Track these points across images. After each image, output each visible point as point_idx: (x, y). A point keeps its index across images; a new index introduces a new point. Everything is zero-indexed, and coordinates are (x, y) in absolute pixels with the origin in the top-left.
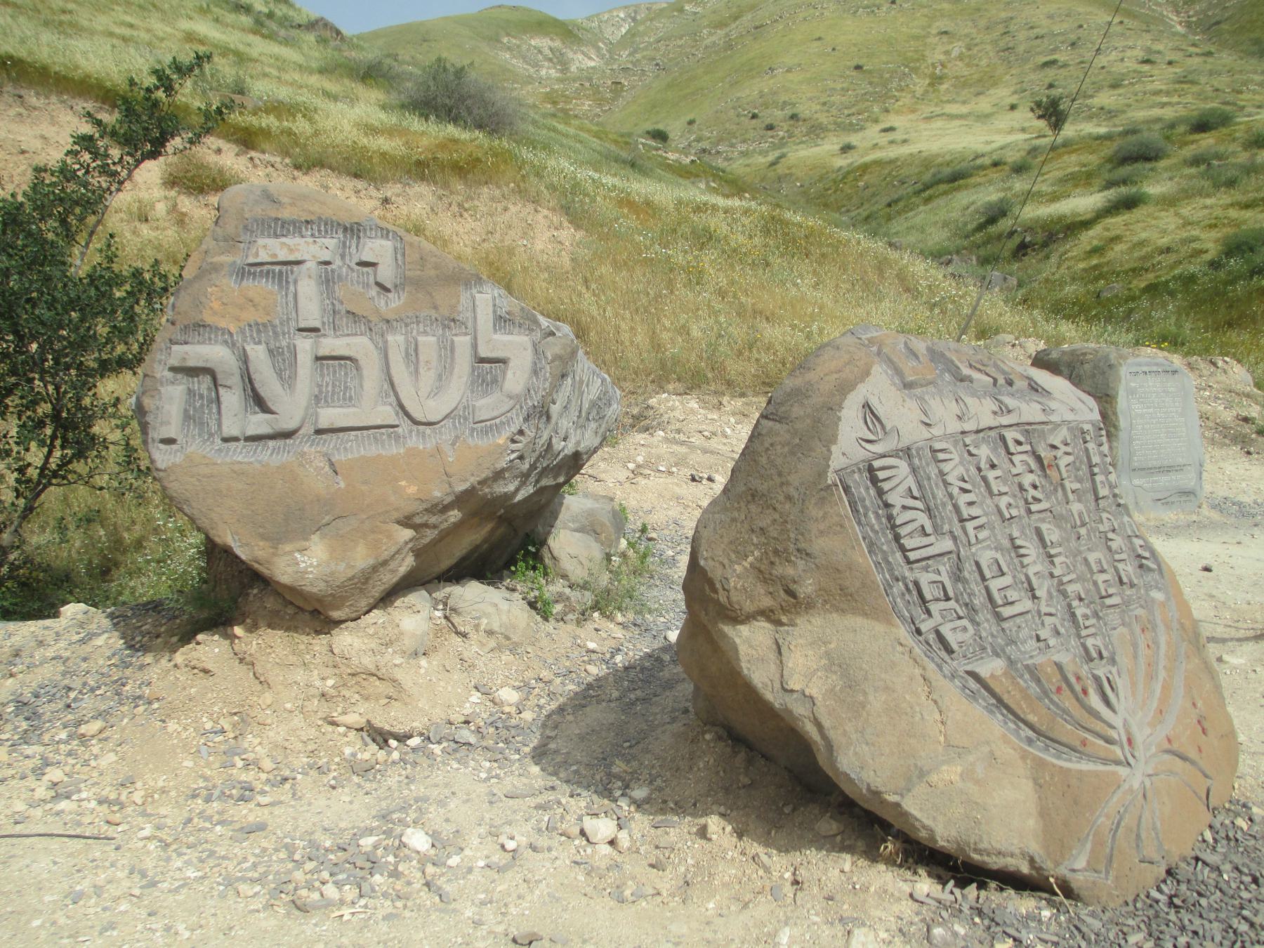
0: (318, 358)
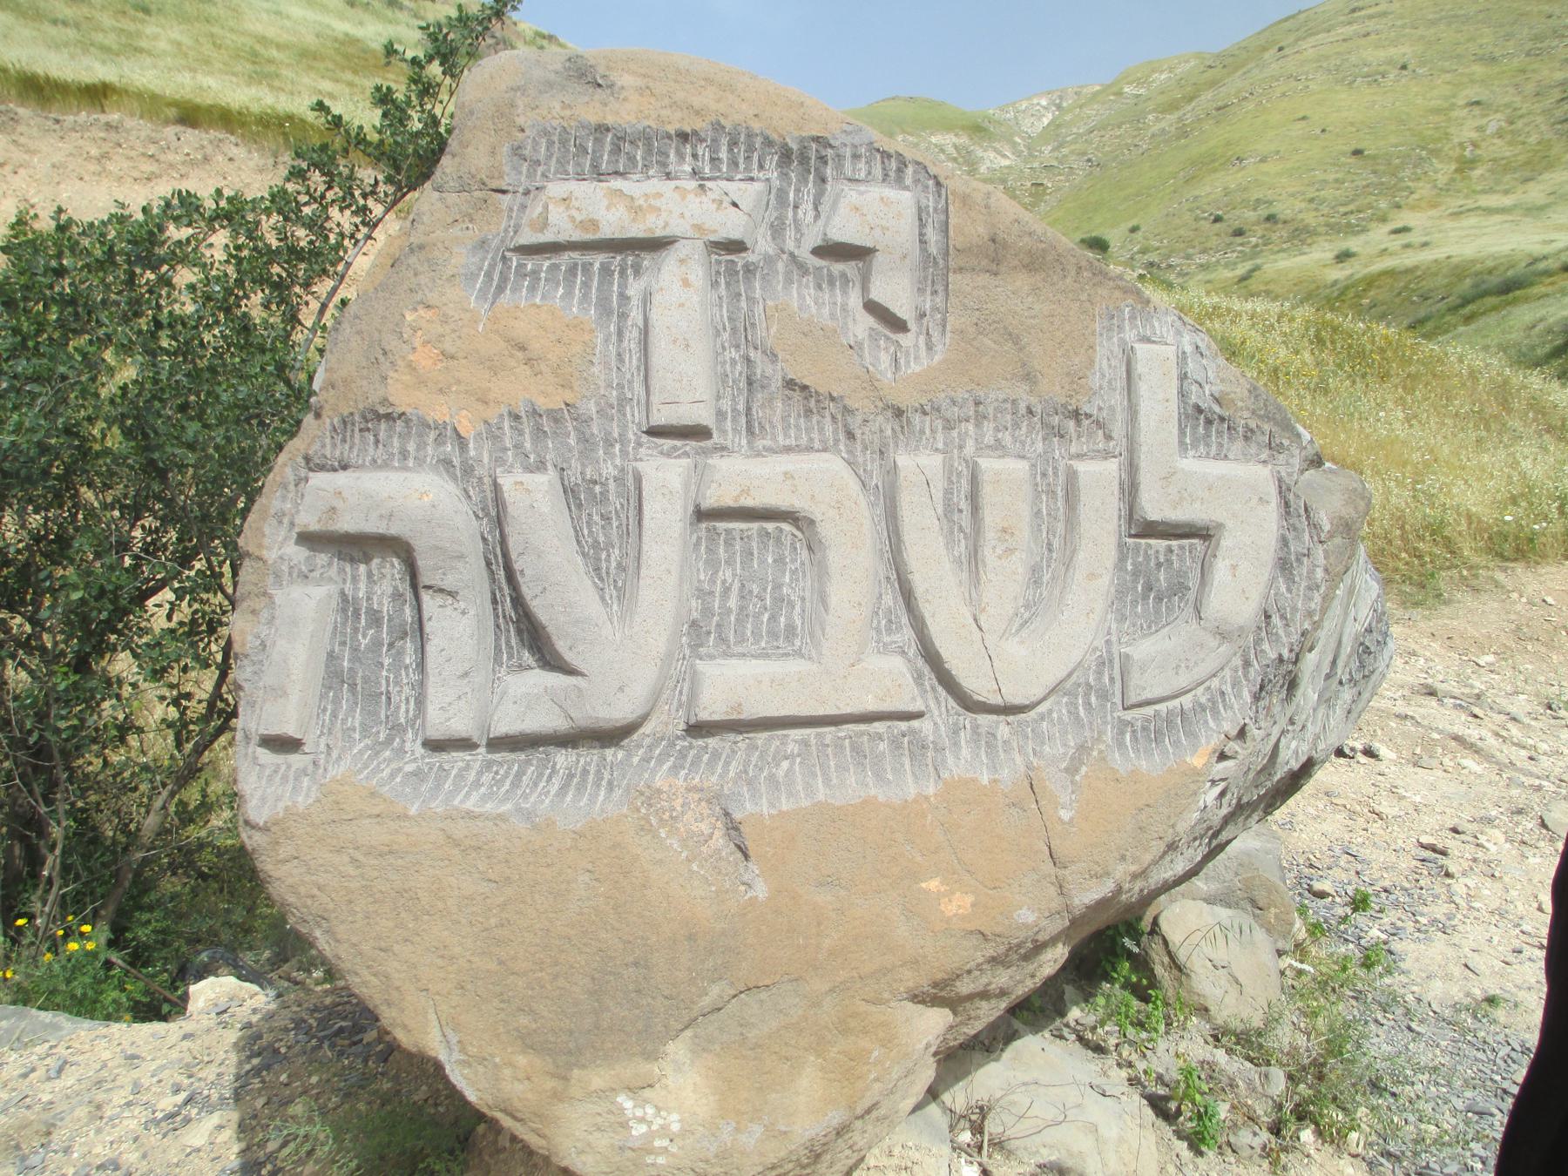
0: (702, 515)
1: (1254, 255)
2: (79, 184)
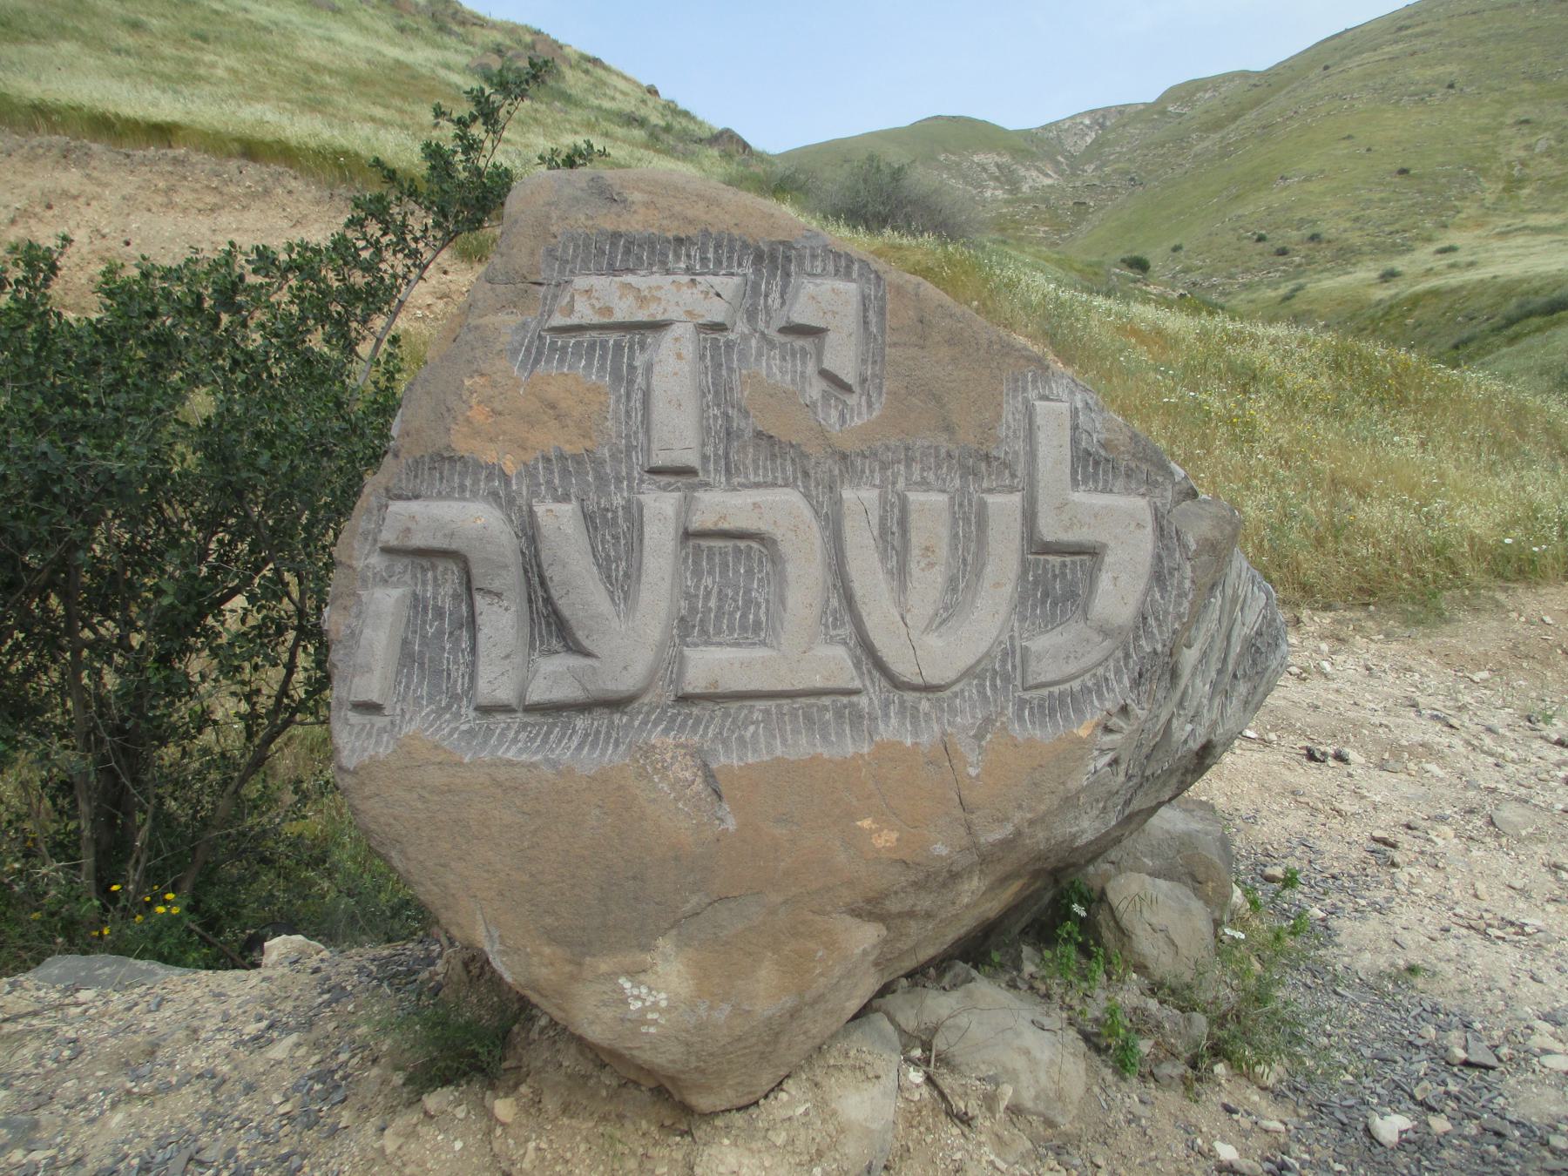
0: (687, 535)
1: (1298, 275)
2: (147, 215)
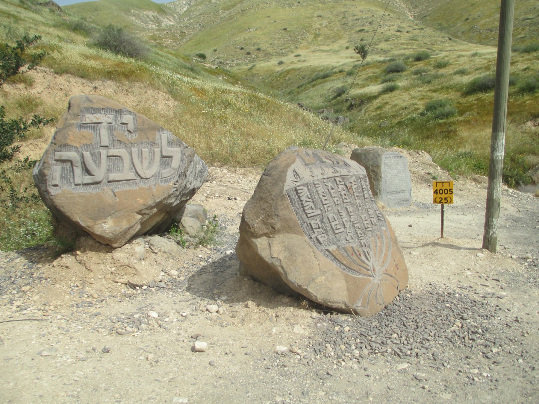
0: (108, 156)
